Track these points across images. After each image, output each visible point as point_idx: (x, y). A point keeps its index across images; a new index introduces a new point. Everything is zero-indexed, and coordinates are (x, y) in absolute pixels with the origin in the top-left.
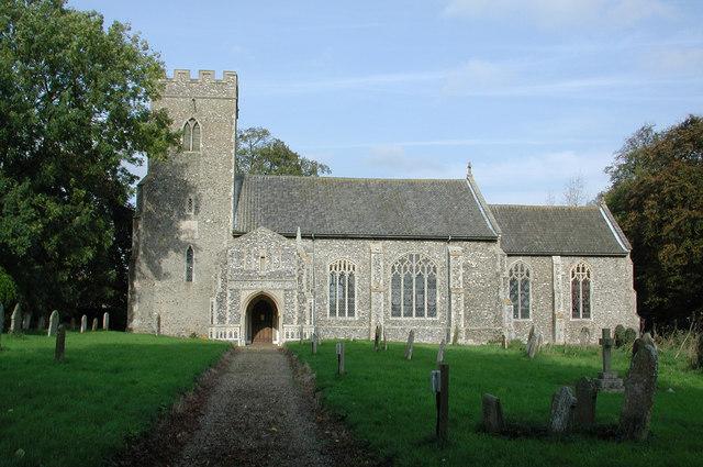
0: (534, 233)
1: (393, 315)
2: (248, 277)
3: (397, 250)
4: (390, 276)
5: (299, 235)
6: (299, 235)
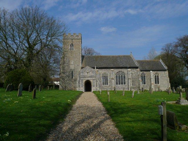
0: (147, 66)
1: (155, 84)
2: (84, 77)
3: (116, 71)
4: (115, 76)
5: (95, 68)
6: (95, 68)
